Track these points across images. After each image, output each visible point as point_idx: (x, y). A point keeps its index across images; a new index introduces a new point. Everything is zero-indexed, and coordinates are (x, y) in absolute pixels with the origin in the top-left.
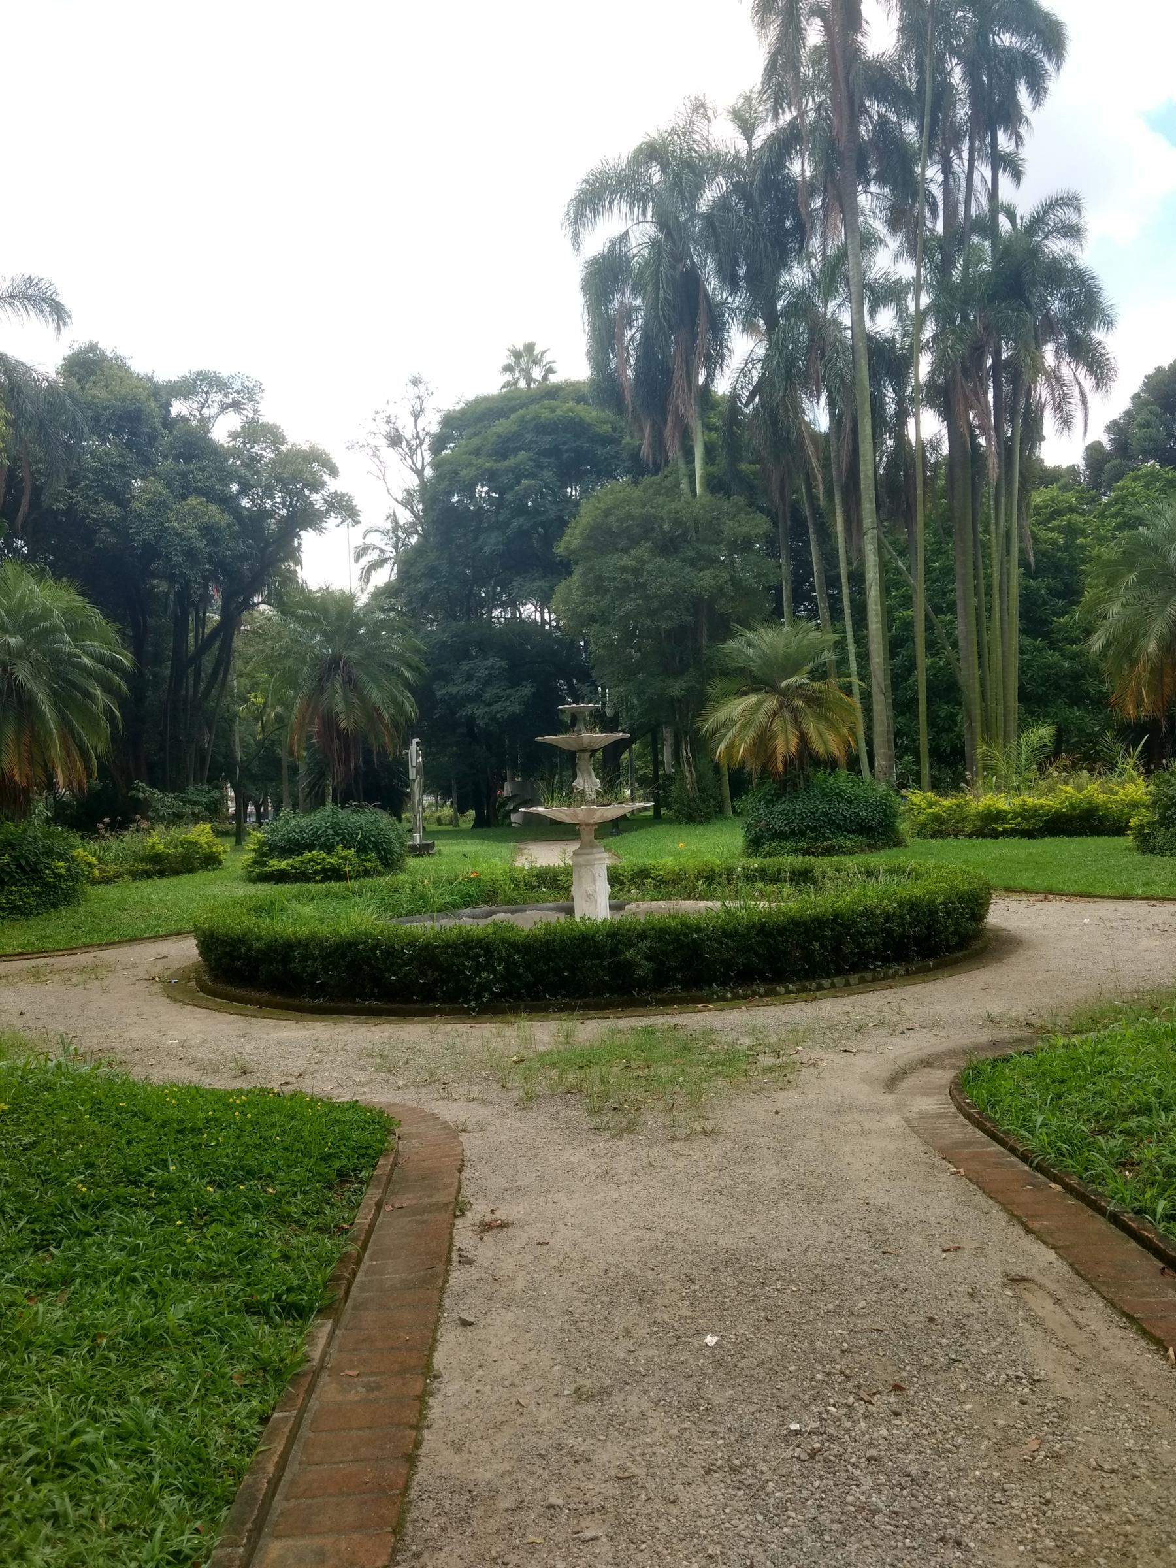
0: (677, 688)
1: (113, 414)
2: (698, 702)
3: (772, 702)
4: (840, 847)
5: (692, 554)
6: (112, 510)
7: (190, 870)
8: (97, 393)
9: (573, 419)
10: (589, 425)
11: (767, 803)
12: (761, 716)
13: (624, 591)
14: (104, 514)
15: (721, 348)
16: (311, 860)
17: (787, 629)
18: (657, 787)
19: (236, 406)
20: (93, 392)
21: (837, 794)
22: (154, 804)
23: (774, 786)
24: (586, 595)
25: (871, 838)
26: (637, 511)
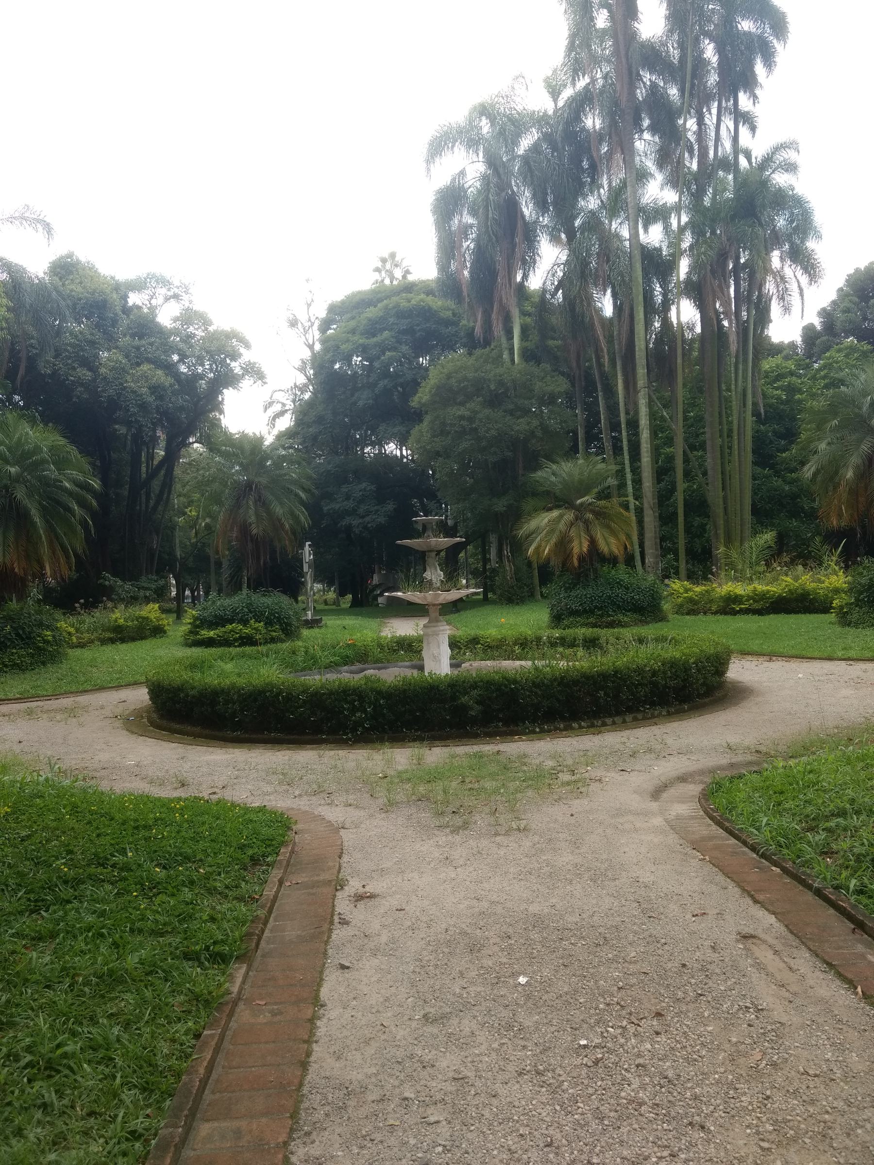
0: (500, 505)
1: (86, 303)
2: (516, 515)
3: (570, 516)
4: (620, 621)
5: (511, 407)
6: (85, 374)
7: (142, 638)
9: (424, 307)
10: (435, 311)
11: (566, 589)
12: (562, 526)
14: (79, 377)
15: (534, 255)
16: (232, 631)
17: (581, 461)
18: (486, 578)
19: (176, 297)
20: (72, 287)
21: (617, 583)
22: (117, 589)
24: (434, 436)
26: (471, 375)
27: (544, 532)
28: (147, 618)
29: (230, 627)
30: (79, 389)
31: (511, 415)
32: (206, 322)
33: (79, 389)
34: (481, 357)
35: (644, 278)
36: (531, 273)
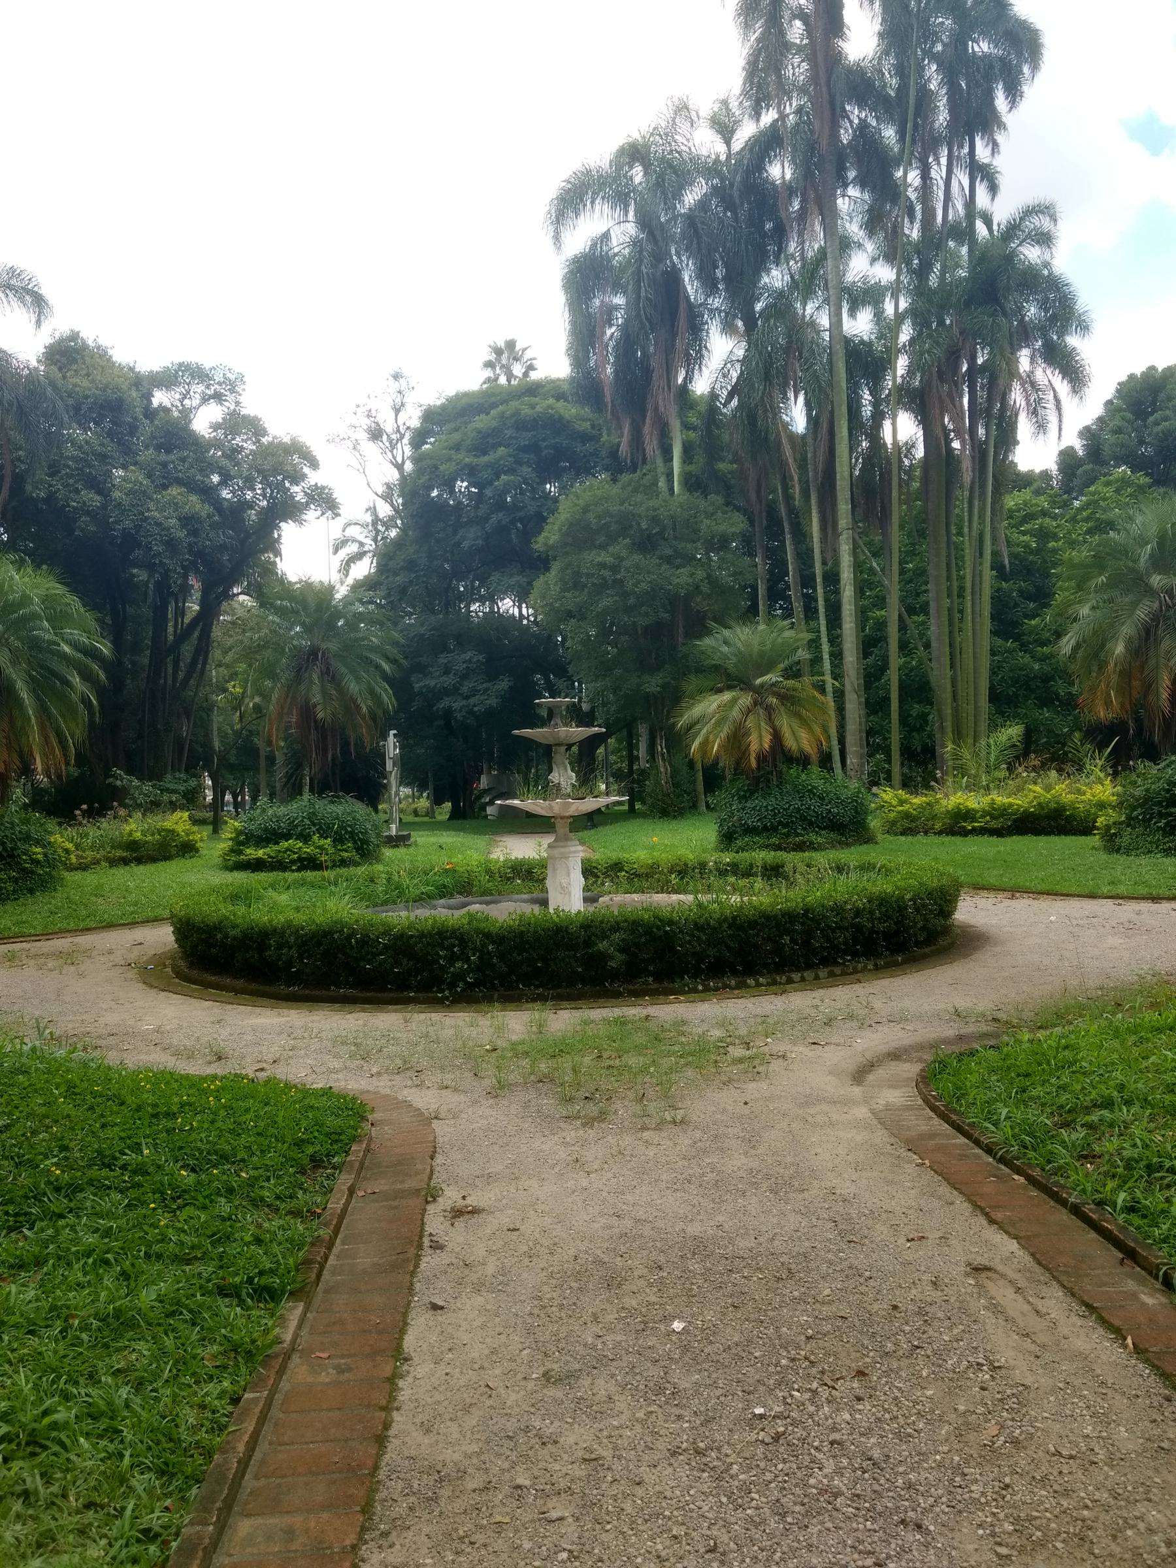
0: (652, 684)
1: (94, 403)
2: (674, 698)
3: (746, 700)
4: (812, 843)
5: (669, 552)
6: (93, 499)
8: (79, 382)
9: (552, 416)
12: (735, 713)
13: (601, 588)
14: (84, 503)
16: (287, 849)
17: (762, 627)
19: (218, 397)
20: (74, 380)
21: (809, 791)
24: (564, 590)
26: (615, 508)
28: (173, 831)
29: (285, 844)
31: (669, 563)
33: (83, 519)
34: (629, 484)
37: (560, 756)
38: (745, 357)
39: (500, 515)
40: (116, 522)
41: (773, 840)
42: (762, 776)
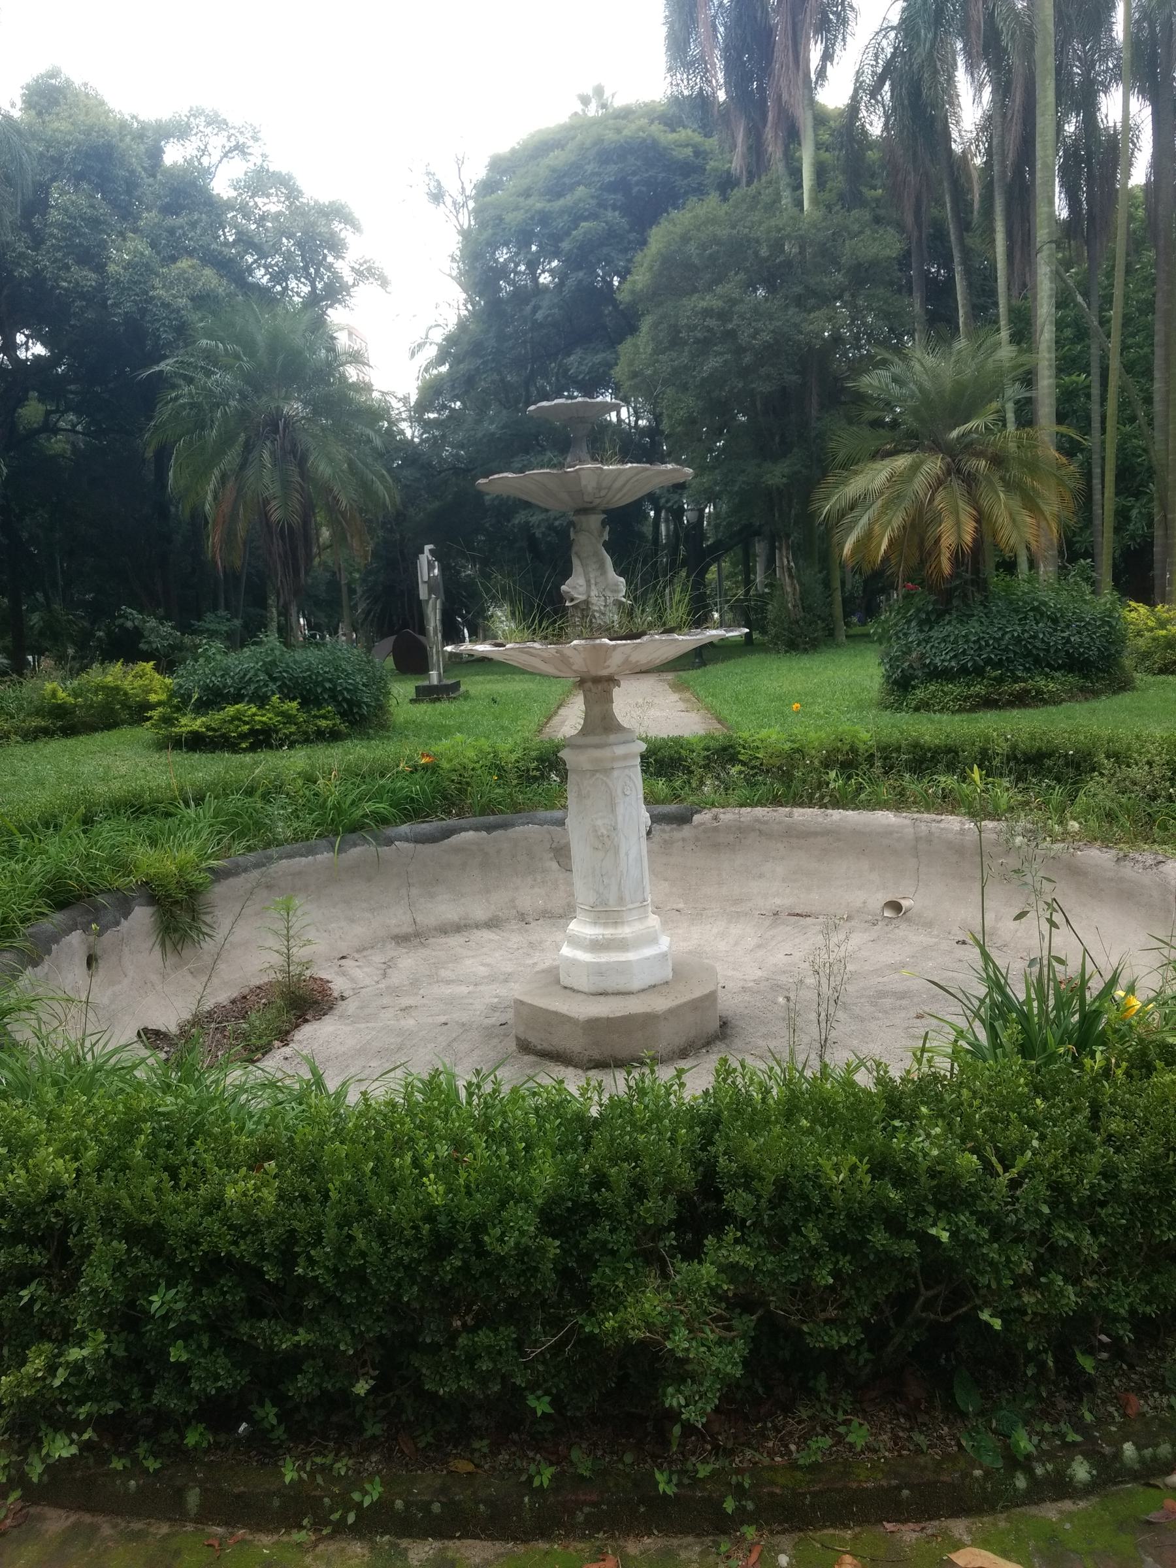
0: (776, 474)
1: (77, 151)
2: (822, 467)
3: (934, 465)
4: (1039, 692)
5: (798, 289)
6: (87, 277)
7: (109, 727)
8: (59, 126)
9: (644, 140)
10: (665, 149)
11: (921, 624)
12: (919, 483)
13: (705, 345)
14: (78, 283)
15: (844, 9)
16: (233, 719)
17: (962, 343)
18: (748, 613)
19: (240, 149)
20: (56, 125)
21: (1033, 609)
22: (146, 633)
23: (933, 598)
24: (656, 352)
25: (1085, 677)
26: (723, 232)
27: (879, 502)
28: (117, 689)
29: (231, 710)
30: (78, 303)
31: (798, 305)
32: (293, 193)
33: (78, 303)
34: (744, 200)
35: (1056, 25)
36: (838, 47)
37: (591, 540)
38: (903, 21)
39: (581, 274)
40: (115, 305)
41: (978, 689)
42: (956, 588)
